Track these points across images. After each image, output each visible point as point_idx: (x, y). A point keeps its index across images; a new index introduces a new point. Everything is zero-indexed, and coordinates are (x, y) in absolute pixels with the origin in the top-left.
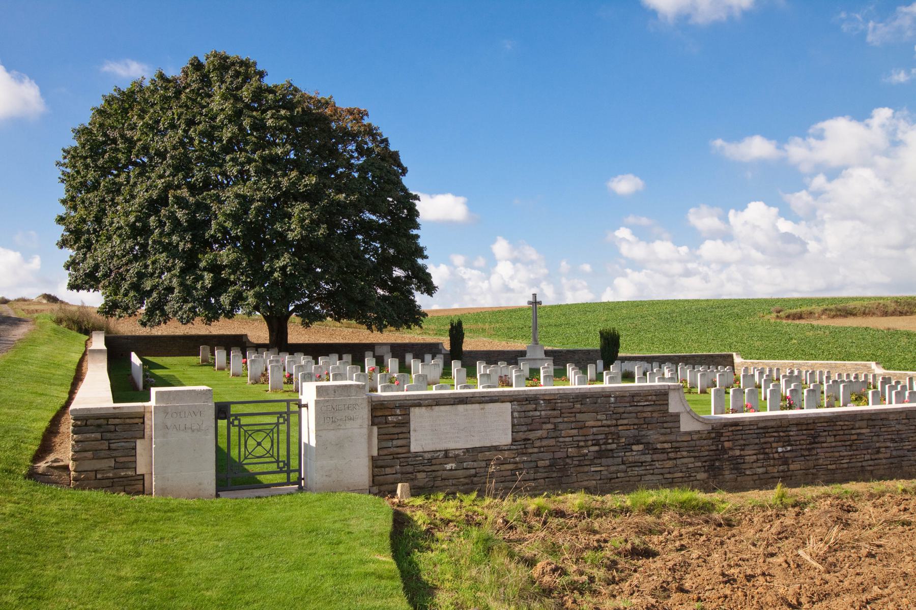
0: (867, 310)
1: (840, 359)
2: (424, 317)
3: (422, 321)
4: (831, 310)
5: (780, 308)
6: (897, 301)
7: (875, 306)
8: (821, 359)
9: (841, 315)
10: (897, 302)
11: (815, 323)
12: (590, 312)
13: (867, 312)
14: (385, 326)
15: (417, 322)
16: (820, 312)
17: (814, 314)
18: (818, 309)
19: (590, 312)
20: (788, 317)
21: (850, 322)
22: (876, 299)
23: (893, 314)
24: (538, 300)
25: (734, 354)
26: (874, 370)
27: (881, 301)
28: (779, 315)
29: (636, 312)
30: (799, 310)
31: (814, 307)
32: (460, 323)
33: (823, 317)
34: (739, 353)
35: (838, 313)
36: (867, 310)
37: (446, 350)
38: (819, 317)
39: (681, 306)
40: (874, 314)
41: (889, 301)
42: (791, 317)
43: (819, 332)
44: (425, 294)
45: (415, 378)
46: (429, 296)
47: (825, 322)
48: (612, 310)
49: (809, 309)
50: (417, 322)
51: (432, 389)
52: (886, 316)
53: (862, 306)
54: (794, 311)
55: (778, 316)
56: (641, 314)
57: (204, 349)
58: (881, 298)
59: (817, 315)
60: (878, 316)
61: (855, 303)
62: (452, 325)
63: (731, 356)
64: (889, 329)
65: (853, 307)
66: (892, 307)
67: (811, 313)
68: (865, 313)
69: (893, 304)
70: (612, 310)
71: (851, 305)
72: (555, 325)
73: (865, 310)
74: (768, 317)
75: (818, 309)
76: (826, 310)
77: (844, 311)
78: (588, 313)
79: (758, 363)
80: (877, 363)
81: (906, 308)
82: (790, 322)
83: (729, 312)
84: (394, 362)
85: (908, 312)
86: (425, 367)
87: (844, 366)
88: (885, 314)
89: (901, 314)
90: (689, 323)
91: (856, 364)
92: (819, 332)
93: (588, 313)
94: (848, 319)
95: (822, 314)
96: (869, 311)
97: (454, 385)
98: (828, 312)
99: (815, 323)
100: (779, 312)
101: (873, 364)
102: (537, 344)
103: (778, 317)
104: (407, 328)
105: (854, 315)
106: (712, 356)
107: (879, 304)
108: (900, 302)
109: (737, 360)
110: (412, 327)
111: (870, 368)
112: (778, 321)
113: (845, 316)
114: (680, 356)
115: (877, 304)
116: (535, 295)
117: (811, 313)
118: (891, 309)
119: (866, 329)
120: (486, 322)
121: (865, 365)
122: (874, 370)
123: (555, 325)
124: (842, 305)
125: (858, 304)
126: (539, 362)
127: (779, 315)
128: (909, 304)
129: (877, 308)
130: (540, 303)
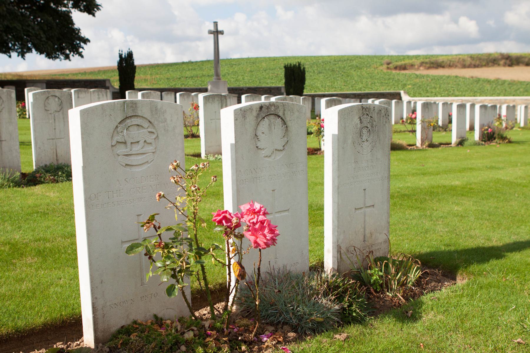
1: (510, 95)
2: (85, 43)
3: (83, 48)
4: (426, 63)
6: (472, 57)
7: (457, 60)
9: (433, 67)
11: (418, 73)
12: (236, 65)
13: (451, 64)
14: (29, 50)
15: (76, 50)
16: (419, 65)
17: (415, 65)
18: (417, 62)
19: (236, 65)
20: (396, 68)
21: (440, 72)
23: (469, 66)
24: (220, 29)
25: (402, 92)
27: (460, 57)
29: (274, 65)
30: (403, 62)
31: (413, 60)
33: (421, 68)
34: (408, 93)
35: (432, 65)
38: (418, 69)
39: (310, 60)
43: (423, 80)
44: (86, 14)
46: (91, 16)
47: (422, 72)
48: (253, 63)
50: (76, 50)
51: (260, 99)
54: (399, 63)
56: (279, 66)
58: (460, 55)
59: (416, 67)
60: (459, 68)
61: (443, 57)
62: (121, 56)
63: (399, 94)
64: (472, 77)
66: (469, 61)
67: (412, 66)
69: (469, 59)
70: (253, 63)
71: (440, 59)
72: (208, 76)
73: (450, 63)
74: (381, 68)
76: (423, 63)
78: (234, 66)
82: (398, 72)
83: (350, 64)
88: (464, 66)
89: (475, 66)
90: (320, 73)
91: (526, 100)
92: (423, 80)
97: (29, 144)
98: (424, 65)
99: (418, 73)
102: (220, 79)
104: (65, 59)
107: (460, 58)
108: (474, 57)
109: (405, 98)
110: (71, 56)
112: (389, 71)
116: (216, 24)
118: (468, 63)
119: (456, 77)
120: (147, 74)
123: (208, 76)
125: (445, 59)
127: (389, 66)
129: (458, 62)
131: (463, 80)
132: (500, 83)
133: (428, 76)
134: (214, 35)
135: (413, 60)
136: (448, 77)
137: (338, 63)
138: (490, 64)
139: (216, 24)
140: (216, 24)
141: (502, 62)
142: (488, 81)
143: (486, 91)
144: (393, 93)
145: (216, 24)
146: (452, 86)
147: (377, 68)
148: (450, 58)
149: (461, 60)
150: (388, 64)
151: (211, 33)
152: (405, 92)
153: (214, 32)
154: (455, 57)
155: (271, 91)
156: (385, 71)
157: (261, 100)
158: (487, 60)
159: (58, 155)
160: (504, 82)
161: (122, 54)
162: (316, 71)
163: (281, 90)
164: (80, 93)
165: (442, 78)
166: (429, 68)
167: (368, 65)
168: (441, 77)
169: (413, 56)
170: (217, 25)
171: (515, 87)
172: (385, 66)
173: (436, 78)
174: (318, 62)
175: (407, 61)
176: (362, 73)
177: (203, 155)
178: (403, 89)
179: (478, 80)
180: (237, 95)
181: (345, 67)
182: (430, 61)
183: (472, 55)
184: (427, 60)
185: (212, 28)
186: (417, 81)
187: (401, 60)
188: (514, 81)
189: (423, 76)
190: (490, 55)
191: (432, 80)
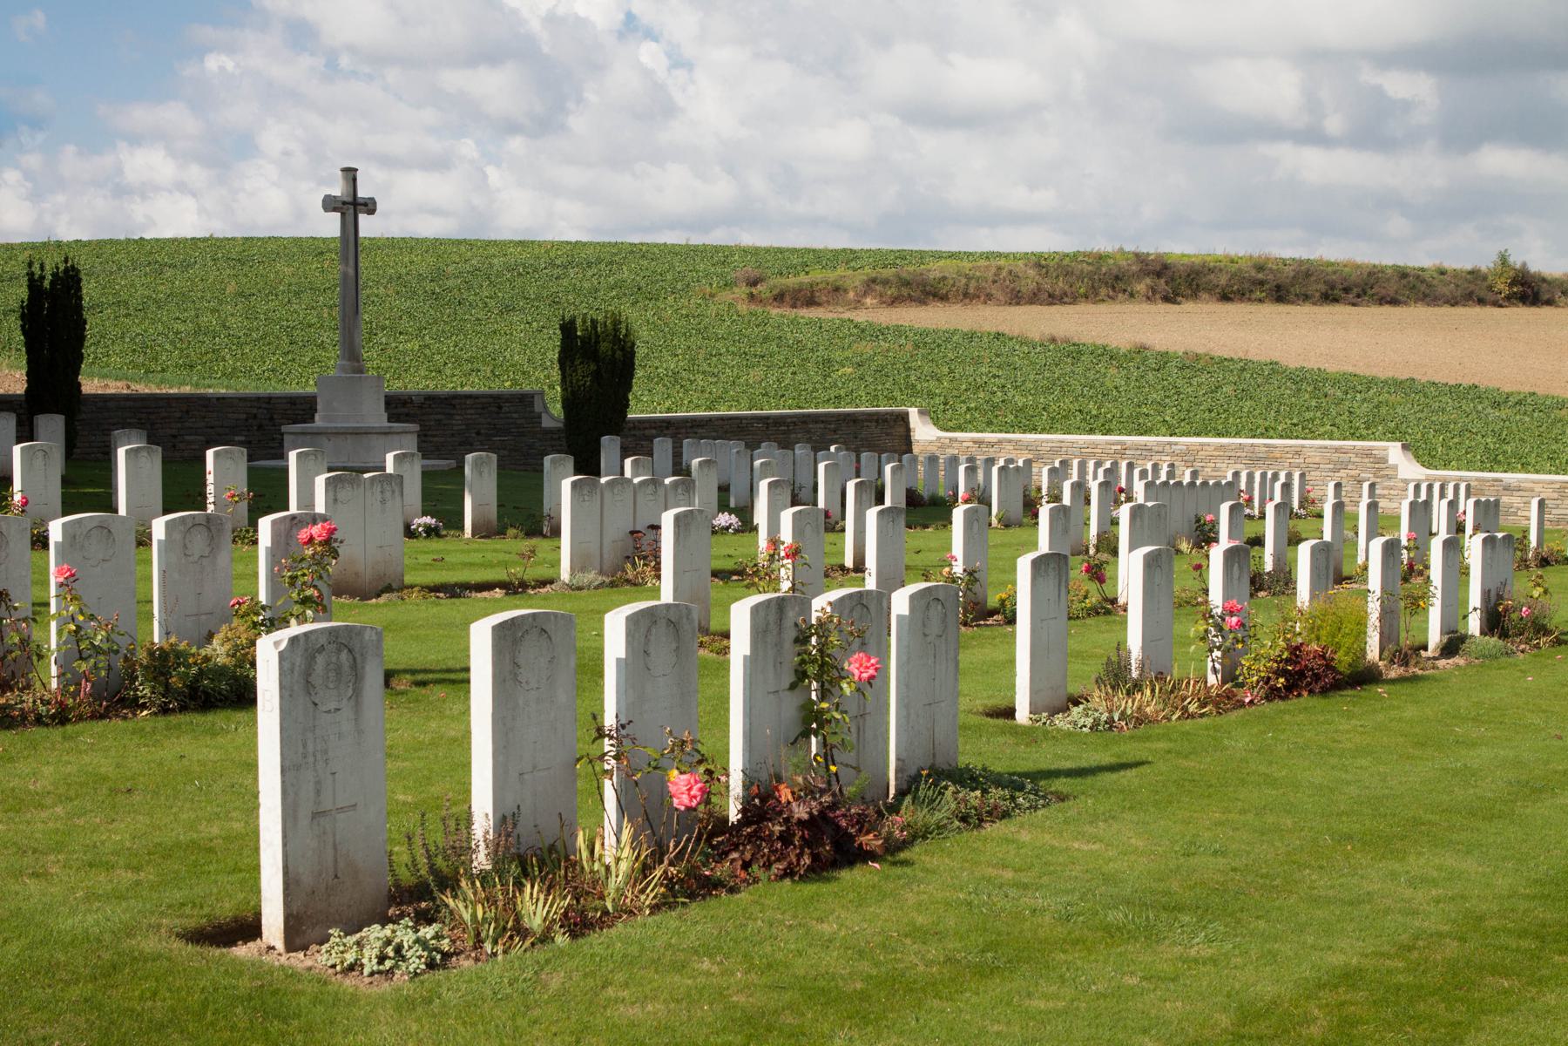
0: (973, 284)
4: (886, 282)
5: (757, 273)
6: (1040, 263)
7: (990, 275)
8: (1194, 434)
9: (911, 298)
10: (1039, 265)
13: (971, 291)
16: (861, 288)
17: (846, 291)
18: (854, 279)
20: (779, 298)
22: (988, 256)
23: (1034, 298)
25: (913, 413)
26: (1395, 468)
27: (1002, 262)
28: (754, 291)
30: (804, 279)
31: (840, 271)
32: (69, 280)
33: (868, 301)
35: (905, 291)
36: (973, 284)
37: (552, 417)
38: (857, 304)
40: (989, 297)
41: (1020, 263)
42: (787, 298)
45: (166, 546)
47: (873, 314)
49: (832, 276)
52: (1018, 304)
53: (959, 273)
54: (792, 281)
55: (752, 297)
57: (477, 464)
59: (851, 295)
61: (942, 263)
63: (903, 419)
65: (939, 275)
68: (967, 296)
69: (1032, 272)
71: (935, 270)
74: (726, 296)
75: (854, 279)
76: (874, 281)
77: (918, 285)
78: (169, 273)
79: (1000, 442)
80: (1405, 447)
81: (1061, 284)
84: (39, 462)
85: (1065, 294)
86: (342, 495)
87: (1298, 453)
88: (1016, 298)
89: (1054, 299)
90: (508, 309)
91: (1337, 450)
93: (169, 273)
94: (929, 308)
95: (865, 294)
96: (978, 288)
99: (861, 317)
100: (754, 283)
101: (1394, 452)
103: (752, 297)
105: (944, 298)
106: (851, 419)
107: (999, 268)
108: (1046, 267)
109: (924, 432)
111: (1384, 460)
113: (922, 302)
114: (767, 417)
115: (993, 270)
116: (350, 174)
117: (837, 289)
118: (1028, 286)
119: (998, 336)
121: (1368, 454)
122: (1395, 468)
124: (911, 269)
126: (377, 441)
127: (754, 291)
128: (1068, 273)
129: (994, 282)
130: (369, 207)
131: (1026, 349)
132: (1152, 362)
133: (899, 331)
134: (343, 214)
135: (840, 271)
136: (971, 336)
137: (566, 275)
138: (1103, 291)
139: (350, 175)
140: (350, 174)
141: (1141, 287)
142: (1109, 355)
143: (1115, 393)
144: (887, 413)
145: (350, 175)
146: (994, 371)
147: (712, 295)
148: (966, 265)
149: (1004, 273)
150: (754, 283)
151: (335, 210)
152: (921, 413)
153: (344, 203)
154: (982, 263)
155: (500, 408)
156: (743, 308)
157: (883, 504)
158: (1091, 275)
159: (936, 743)
160: (1164, 358)
161: (42, 278)
162: (492, 303)
163: (532, 404)
164: (340, 485)
165: (948, 340)
166: (894, 301)
167: (679, 286)
168: (949, 335)
169: (836, 254)
170: (355, 180)
171: (1203, 378)
172: (742, 291)
173: (928, 340)
174: (491, 266)
175: (817, 275)
176: (663, 314)
177: (1023, 715)
178: (913, 393)
179: (1076, 352)
180: (414, 427)
181: (596, 291)
182: (898, 276)
183: (1040, 256)
184: (889, 273)
185: (337, 190)
186: (866, 348)
187: (792, 269)
188: (1198, 357)
189: (880, 333)
190: (1101, 258)
191: (917, 346)
